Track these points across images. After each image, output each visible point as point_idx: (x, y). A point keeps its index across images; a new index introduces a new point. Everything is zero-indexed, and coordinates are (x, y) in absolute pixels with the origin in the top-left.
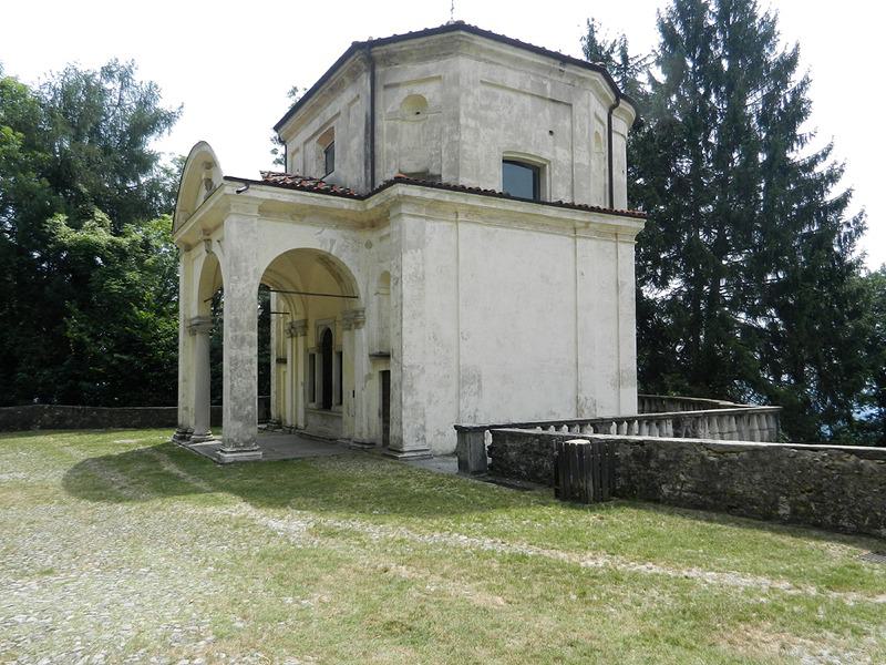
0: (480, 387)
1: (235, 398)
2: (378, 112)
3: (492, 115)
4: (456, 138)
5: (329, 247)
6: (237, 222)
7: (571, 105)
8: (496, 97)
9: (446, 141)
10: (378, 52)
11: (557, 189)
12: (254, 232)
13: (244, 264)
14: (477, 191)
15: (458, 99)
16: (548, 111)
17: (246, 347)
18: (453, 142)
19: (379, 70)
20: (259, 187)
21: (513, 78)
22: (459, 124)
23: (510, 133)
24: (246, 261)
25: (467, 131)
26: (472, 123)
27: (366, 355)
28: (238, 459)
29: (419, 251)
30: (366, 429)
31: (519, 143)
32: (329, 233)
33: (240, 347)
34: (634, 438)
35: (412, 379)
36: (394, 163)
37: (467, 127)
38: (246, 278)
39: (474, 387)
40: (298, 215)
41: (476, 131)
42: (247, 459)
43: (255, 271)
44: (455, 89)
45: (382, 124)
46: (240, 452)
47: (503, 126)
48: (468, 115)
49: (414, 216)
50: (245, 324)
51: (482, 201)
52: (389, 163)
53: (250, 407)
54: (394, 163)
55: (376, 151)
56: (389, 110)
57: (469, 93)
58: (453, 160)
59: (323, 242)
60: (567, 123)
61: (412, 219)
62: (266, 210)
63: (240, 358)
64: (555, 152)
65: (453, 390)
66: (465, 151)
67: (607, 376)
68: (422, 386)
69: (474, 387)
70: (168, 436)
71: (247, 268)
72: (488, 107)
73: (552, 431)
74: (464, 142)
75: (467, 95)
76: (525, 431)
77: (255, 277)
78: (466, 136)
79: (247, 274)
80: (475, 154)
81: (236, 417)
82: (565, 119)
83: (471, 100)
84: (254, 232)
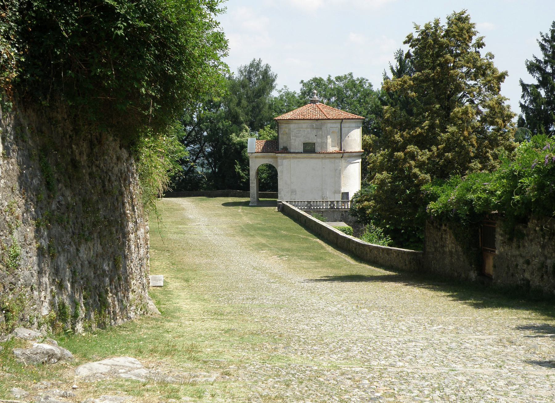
11: (318, 149)
21: (304, 126)
32: (270, 160)
40: (263, 157)
41: (295, 140)
62: (256, 157)
68: (282, 193)
78: (292, 141)
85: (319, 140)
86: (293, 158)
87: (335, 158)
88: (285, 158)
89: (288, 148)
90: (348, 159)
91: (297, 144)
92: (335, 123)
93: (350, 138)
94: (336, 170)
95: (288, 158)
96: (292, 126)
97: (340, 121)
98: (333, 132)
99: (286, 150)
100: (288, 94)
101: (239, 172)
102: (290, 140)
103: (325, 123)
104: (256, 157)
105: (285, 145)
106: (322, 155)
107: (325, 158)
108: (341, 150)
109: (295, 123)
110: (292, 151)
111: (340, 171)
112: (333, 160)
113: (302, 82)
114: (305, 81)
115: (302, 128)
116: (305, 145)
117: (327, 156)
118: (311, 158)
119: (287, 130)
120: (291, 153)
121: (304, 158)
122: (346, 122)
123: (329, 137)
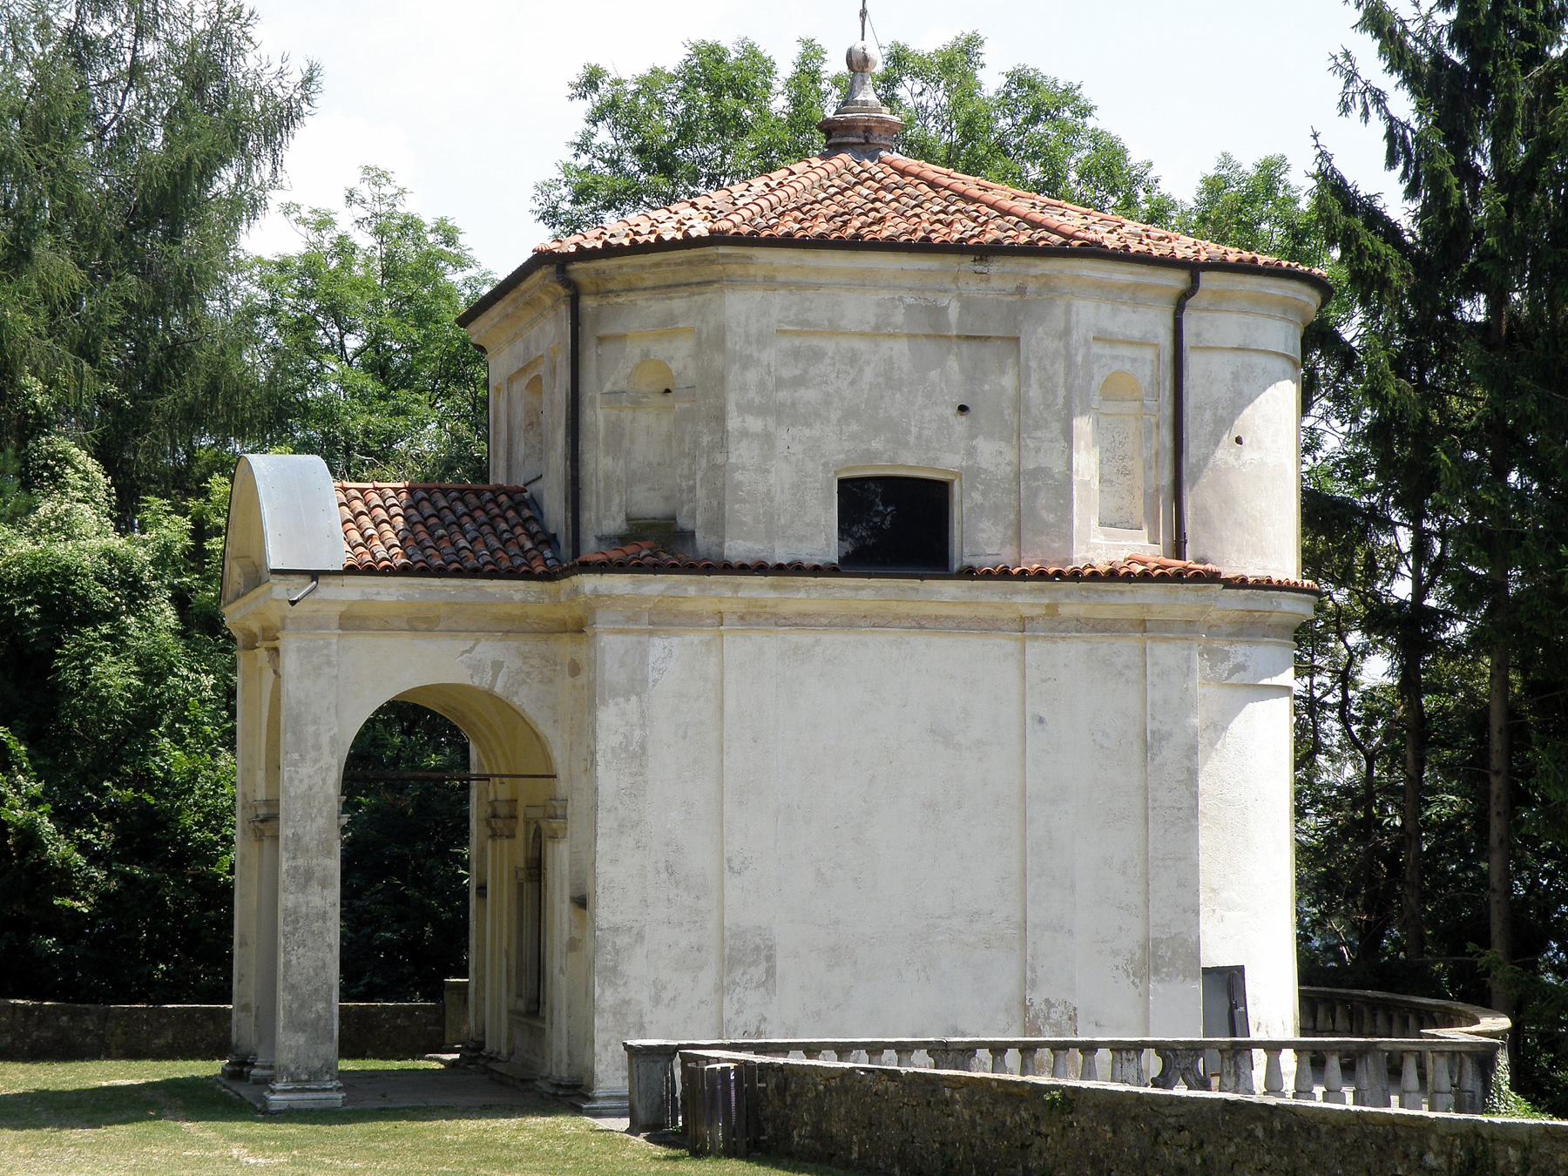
0: (770, 972)
1: (293, 986)
2: (589, 390)
3: (809, 395)
4: (720, 459)
5: (488, 677)
6: (299, 650)
7: (1017, 339)
8: (817, 355)
9: (704, 462)
10: (576, 267)
11: (977, 533)
12: (329, 663)
13: (311, 729)
14: (761, 569)
15: (722, 380)
16: (952, 369)
17: (315, 887)
18: (715, 468)
19: (588, 303)
20: (337, 580)
21: (858, 309)
22: (724, 431)
23: (854, 427)
24: (315, 722)
25: (744, 444)
26: (755, 424)
27: (567, 900)
28: (295, 1105)
29: (634, 698)
30: (565, 1054)
31: (876, 445)
32: (489, 649)
33: (303, 888)
34: (1044, 1080)
35: (617, 952)
36: (617, 500)
37: (745, 434)
38: (313, 754)
39: (758, 972)
40: (421, 623)
41: (767, 438)
42: (311, 1105)
43: (333, 740)
44: (718, 360)
45: (596, 417)
46: (303, 1090)
47: (834, 417)
48: (746, 409)
49: (621, 632)
50: (313, 845)
51: (773, 587)
52: (609, 500)
53: (320, 1006)
54: (617, 500)
55: (582, 473)
56: (608, 387)
57: (747, 363)
58: (715, 503)
59: (476, 668)
60: (1008, 381)
61: (620, 637)
62: (351, 622)
63: (304, 909)
64: (971, 452)
65: (708, 977)
66: (739, 485)
67: (1115, 953)
68: (636, 966)
69: (758, 972)
70: (210, 1068)
71: (317, 735)
72: (799, 382)
73: (889, 1061)
74: (736, 468)
75: (745, 367)
76: (767, 1059)
77: (332, 753)
78: (742, 454)
79: (317, 747)
80: (762, 488)
81: (296, 1025)
82: (1003, 372)
83: (752, 376)
84: (329, 663)
85: (992, 454)
86: (751, 618)
87: (1142, 626)
88: (664, 620)
89: (696, 519)
90: (1239, 652)
91: (783, 491)
92: (1134, 296)
93: (1248, 453)
94: (1149, 744)
95: (693, 621)
96: (740, 308)
97: (1176, 280)
98: (1110, 391)
99: (661, 546)
100: (396, 228)
101: (29, 837)
102: (722, 444)
103: (1048, 286)
104: (351, 622)
105: (651, 505)
106: (1026, 599)
107: (1056, 625)
108: (1178, 550)
109: (770, 283)
110: (737, 548)
111: (1192, 750)
112: (1125, 648)
113: (592, 80)
114: (628, 65)
115: (835, 331)
116: (857, 497)
117: (1074, 602)
118: (920, 624)
119: (679, 356)
120: (727, 568)
121: (849, 623)
122: (1221, 302)
123: (1083, 426)
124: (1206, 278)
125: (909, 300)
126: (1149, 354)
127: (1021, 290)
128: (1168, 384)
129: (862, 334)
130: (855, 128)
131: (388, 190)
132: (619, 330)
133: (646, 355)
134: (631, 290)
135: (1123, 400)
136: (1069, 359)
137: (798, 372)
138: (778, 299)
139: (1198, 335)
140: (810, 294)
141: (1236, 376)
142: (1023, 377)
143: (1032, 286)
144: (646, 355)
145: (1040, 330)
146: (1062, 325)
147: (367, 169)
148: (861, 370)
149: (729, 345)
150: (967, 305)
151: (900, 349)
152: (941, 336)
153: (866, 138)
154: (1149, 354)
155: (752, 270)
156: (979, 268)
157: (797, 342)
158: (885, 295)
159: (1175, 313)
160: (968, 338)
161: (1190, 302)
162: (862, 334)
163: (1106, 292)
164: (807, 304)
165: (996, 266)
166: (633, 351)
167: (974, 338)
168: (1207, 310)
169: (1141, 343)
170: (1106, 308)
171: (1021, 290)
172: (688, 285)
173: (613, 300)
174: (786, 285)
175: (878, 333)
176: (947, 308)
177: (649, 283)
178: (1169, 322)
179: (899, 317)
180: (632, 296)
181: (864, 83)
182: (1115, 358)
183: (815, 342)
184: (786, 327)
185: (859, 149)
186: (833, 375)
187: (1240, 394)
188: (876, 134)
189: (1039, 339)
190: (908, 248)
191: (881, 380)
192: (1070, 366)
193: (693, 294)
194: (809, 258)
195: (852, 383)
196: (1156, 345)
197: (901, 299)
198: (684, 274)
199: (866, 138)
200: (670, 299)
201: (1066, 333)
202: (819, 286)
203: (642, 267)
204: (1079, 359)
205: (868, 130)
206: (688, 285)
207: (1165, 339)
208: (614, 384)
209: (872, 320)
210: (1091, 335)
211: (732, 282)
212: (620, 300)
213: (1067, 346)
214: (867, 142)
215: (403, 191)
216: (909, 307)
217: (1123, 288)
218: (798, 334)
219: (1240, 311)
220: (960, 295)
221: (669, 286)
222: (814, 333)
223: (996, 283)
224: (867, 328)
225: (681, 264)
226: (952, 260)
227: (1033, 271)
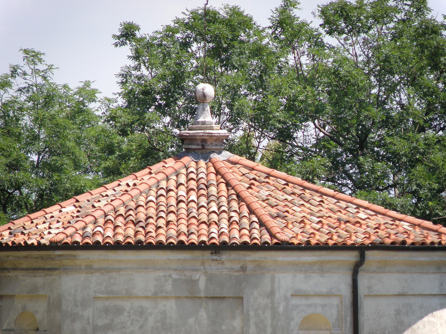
7: (242, 298)
8: (119, 311)
21: (144, 282)
75: (74, 321)
92: (322, 269)
97: (351, 257)
103: (260, 266)
113: (128, 33)
114: (150, 27)
115: (130, 296)
122: (383, 267)
124: (369, 254)
125: (175, 276)
126: (335, 301)
127: (243, 269)
128: (349, 319)
129: (147, 297)
130: (195, 140)
131: (41, 67)
132: (10, 293)
133: (24, 308)
134: (15, 269)
135: (321, 329)
136: (274, 310)
137: (107, 321)
138: (95, 278)
139: (369, 288)
140: (114, 274)
141: (398, 312)
142: (246, 321)
143: (250, 266)
144: (24, 308)
145: (256, 292)
146: (269, 289)
147: (26, 51)
148: (146, 319)
149: (64, 307)
150: (210, 279)
151: (170, 306)
152: (195, 297)
153: (203, 146)
154: (335, 301)
155: (78, 262)
156: (215, 257)
157: (107, 303)
158: (161, 273)
159: (353, 276)
160: (212, 298)
161: (360, 269)
162: (147, 297)
163: (298, 267)
164: (112, 281)
165: (225, 256)
166: (18, 305)
167: (216, 298)
168: (374, 272)
169: (329, 295)
170: (300, 277)
171: (243, 269)
172: (44, 269)
173: (7, 274)
174: (99, 270)
175: (155, 297)
176: (198, 280)
177: (25, 266)
178: (349, 280)
179: (169, 287)
180: (16, 273)
181: (204, 110)
182: (310, 306)
183: (118, 303)
184: (99, 295)
185: (199, 152)
186: (129, 323)
187: (402, 323)
188: (209, 143)
189: (255, 298)
190: (170, 247)
191: (159, 324)
192: (275, 314)
193: (46, 275)
194: (112, 255)
195: (141, 327)
196: (340, 296)
197: (170, 276)
198: (41, 264)
199: (203, 146)
200: (36, 276)
201: (272, 294)
202: (119, 270)
203: (19, 257)
204: (281, 309)
205: (204, 141)
206: (44, 269)
207: (345, 290)
208: (9, 324)
209: (153, 289)
210: (289, 294)
211: (66, 270)
212: (10, 274)
213: (272, 302)
214: (203, 147)
215: (50, 67)
216: (175, 281)
217: (312, 264)
218: (107, 299)
219: (398, 272)
220: (206, 272)
221: (34, 269)
222: (118, 298)
223: (228, 265)
224: (149, 294)
225: (37, 258)
226: (198, 254)
227: (248, 258)
